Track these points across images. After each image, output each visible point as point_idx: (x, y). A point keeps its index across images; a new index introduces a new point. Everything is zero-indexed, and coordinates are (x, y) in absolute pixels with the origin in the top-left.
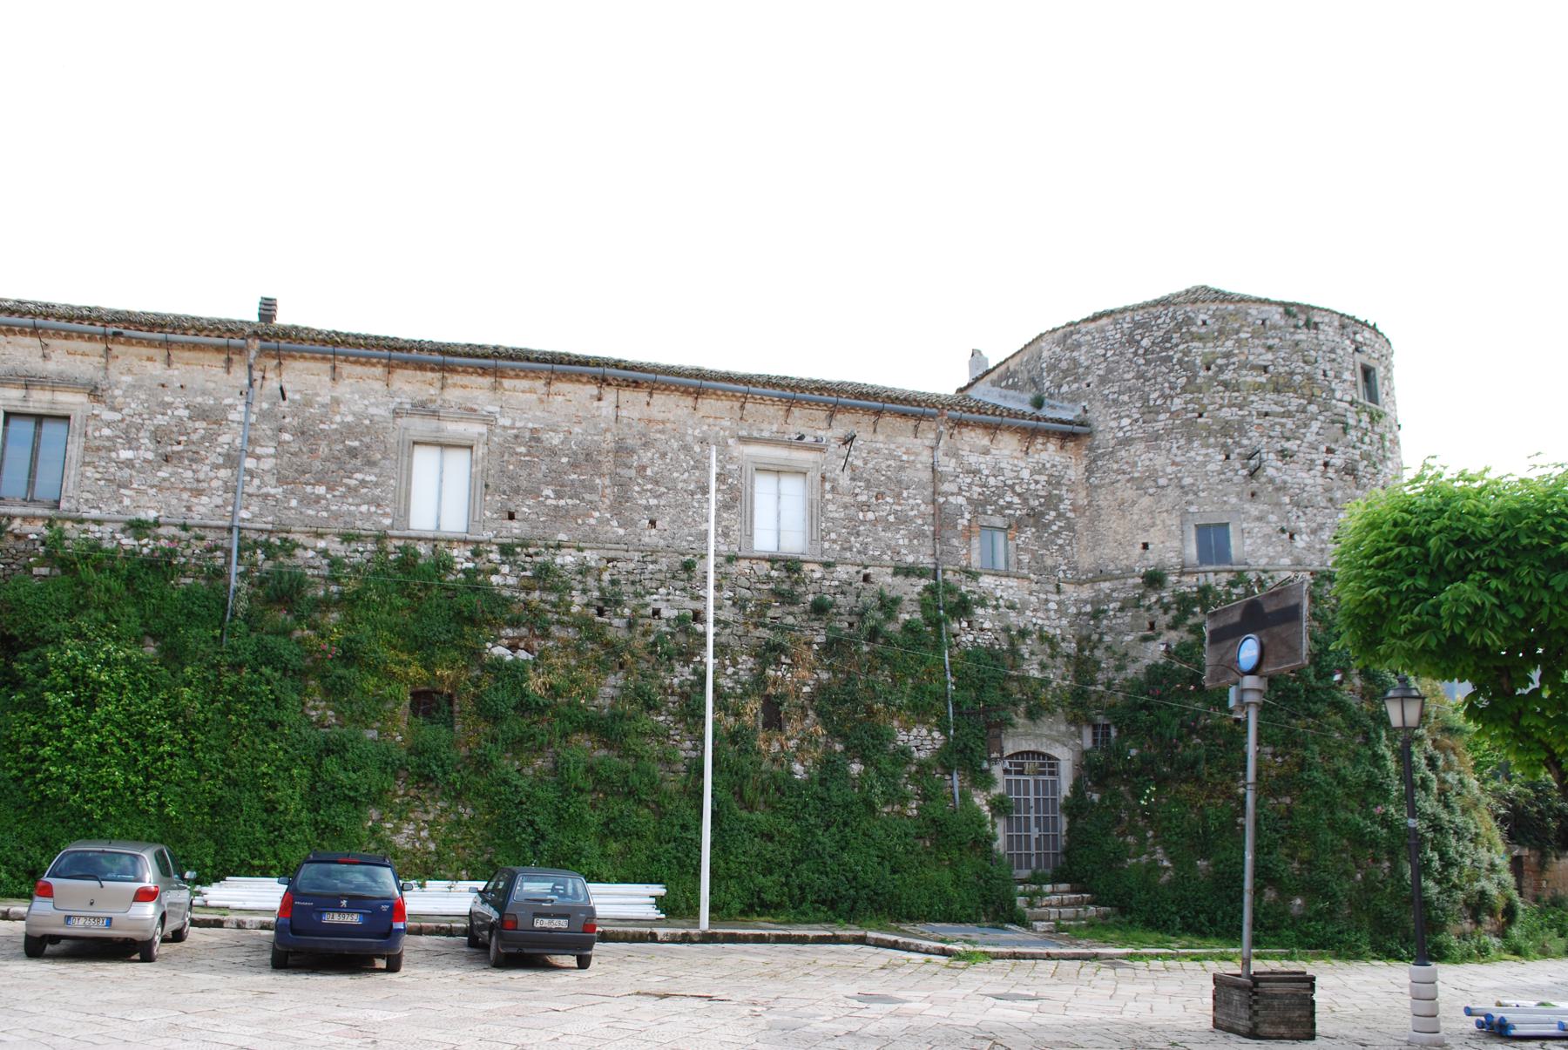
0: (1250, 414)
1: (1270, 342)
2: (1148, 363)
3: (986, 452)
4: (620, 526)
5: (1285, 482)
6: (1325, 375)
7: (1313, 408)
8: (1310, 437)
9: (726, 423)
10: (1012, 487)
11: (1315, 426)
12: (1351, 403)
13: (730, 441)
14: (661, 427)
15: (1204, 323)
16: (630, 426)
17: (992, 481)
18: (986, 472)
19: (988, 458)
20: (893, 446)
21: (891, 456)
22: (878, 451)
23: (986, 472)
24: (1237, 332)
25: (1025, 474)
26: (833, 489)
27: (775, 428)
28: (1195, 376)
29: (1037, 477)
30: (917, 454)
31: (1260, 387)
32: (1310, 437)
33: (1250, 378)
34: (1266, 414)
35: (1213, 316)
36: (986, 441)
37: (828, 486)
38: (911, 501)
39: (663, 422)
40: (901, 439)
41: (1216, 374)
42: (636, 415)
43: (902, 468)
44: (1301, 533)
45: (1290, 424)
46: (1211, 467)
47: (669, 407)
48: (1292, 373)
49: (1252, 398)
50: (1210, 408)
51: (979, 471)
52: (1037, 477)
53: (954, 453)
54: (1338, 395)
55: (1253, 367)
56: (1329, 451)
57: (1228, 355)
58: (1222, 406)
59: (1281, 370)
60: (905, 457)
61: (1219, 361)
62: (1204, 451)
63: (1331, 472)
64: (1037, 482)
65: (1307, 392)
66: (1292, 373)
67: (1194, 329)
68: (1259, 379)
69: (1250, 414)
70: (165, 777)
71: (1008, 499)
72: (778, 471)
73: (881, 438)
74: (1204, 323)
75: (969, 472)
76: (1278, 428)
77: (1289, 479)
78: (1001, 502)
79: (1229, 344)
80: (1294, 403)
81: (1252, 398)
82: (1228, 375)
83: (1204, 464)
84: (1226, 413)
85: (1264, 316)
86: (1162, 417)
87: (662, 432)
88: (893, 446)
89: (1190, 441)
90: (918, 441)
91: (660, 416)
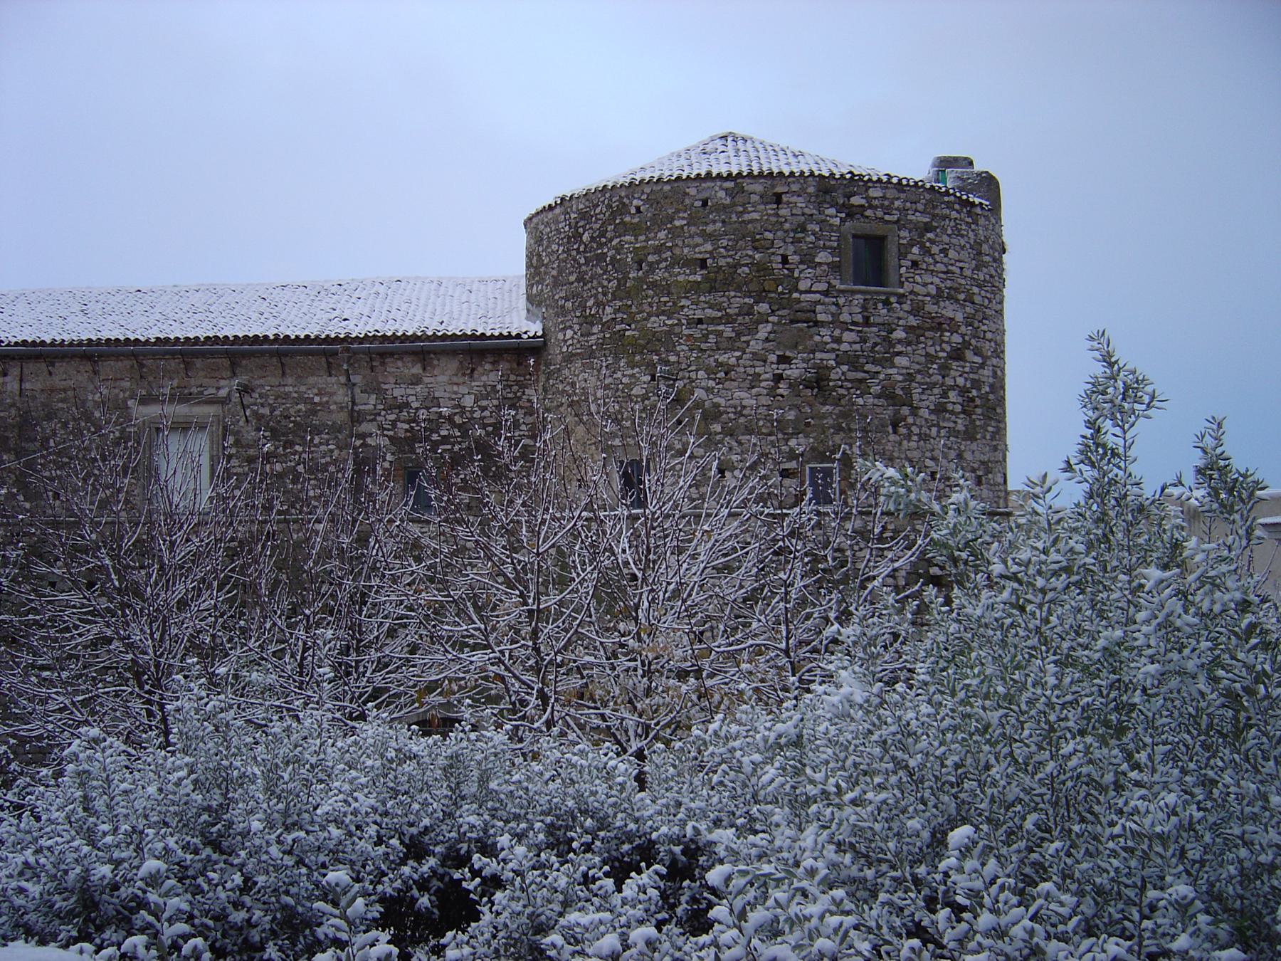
0: (680, 324)
1: (710, 228)
2: (588, 261)
3: (416, 381)
4: (26, 500)
5: (717, 406)
6: (785, 260)
7: (764, 307)
8: (755, 346)
9: (126, 384)
10: (450, 419)
11: (763, 331)
12: (826, 293)
13: (130, 403)
14: (63, 395)
15: (638, 209)
16: (34, 398)
17: (423, 414)
18: (415, 405)
19: (418, 388)
20: (303, 389)
21: (302, 399)
22: (287, 395)
23: (415, 405)
24: (671, 219)
25: (468, 401)
26: (237, 443)
27: (175, 383)
28: (626, 278)
29: (484, 403)
30: (331, 394)
31: (695, 287)
32: (755, 346)
33: (684, 276)
34: (700, 321)
35: (646, 201)
36: (417, 370)
37: (231, 440)
38: (323, 448)
39: (65, 390)
40: (312, 380)
41: (647, 274)
42: (39, 386)
43: (314, 413)
44: (733, 469)
45: (728, 331)
46: (637, 391)
47: (69, 376)
48: (737, 265)
49: (684, 302)
50: (638, 317)
51: (407, 405)
52: (484, 403)
53: (374, 388)
54: (803, 285)
55: (688, 263)
56: (783, 360)
57: (659, 250)
58: (650, 315)
59: (722, 262)
60: (317, 399)
61: (650, 258)
62: (629, 372)
63: (783, 389)
64: (483, 409)
65: (754, 287)
66: (737, 265)
67: (627, 219)
68: (692, 278)
69: (680, 324)
70: (1050, 595)
71: (444, 433)
72: (183, 427)
73: (290, 380)
74: (638, 209)
75: (390, 408)
76: (712, 338)
77: (722, 401)
78: (435, 437)
79: (662, 235)
80: (737, 301)
81: (684, 302)
82: (658, 275)
83: (629, 386)
84: (655, 323)
85: (705, 195)
86: (595, 330)
87: (63, 401)
88: (303, 389)
89: (617, 359)
90: (334, 379)
91: (62, 384)
